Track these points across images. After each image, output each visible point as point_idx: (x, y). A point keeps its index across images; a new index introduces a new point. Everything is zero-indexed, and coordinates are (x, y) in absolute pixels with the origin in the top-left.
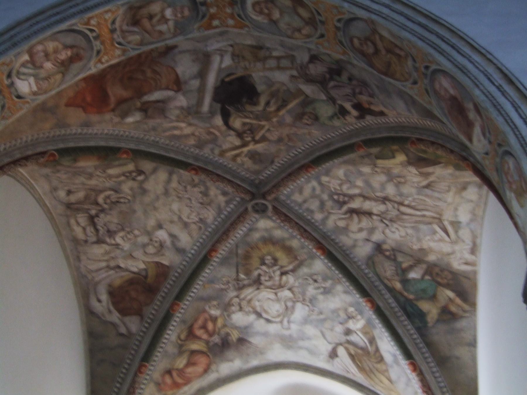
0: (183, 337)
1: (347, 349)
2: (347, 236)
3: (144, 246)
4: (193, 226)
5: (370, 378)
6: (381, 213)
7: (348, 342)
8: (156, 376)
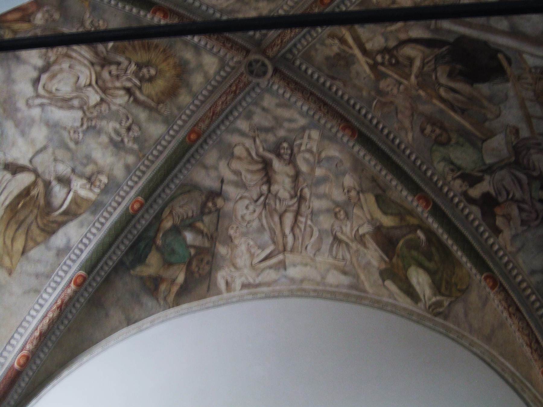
1: (34, 184)
2: (220, 158)
6: (274, 193)
7: (47, 185)
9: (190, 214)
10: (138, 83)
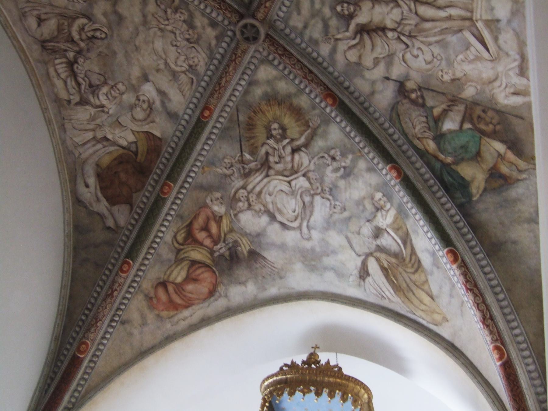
0: (180, 238)
1: (378, 260)
2: (363, 77)
3: (132, 107)
4: (183, 77)
5: (408, 299)
6: (396, 26)
7: (380, 249)
8: (147, 285)
9: (424, 119)
10: (287, 141)
